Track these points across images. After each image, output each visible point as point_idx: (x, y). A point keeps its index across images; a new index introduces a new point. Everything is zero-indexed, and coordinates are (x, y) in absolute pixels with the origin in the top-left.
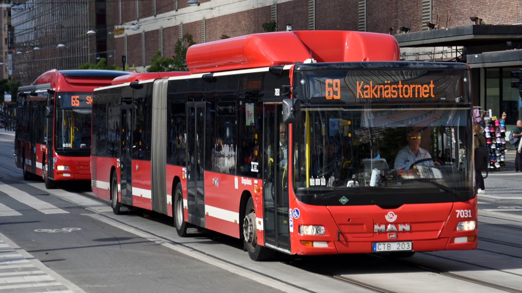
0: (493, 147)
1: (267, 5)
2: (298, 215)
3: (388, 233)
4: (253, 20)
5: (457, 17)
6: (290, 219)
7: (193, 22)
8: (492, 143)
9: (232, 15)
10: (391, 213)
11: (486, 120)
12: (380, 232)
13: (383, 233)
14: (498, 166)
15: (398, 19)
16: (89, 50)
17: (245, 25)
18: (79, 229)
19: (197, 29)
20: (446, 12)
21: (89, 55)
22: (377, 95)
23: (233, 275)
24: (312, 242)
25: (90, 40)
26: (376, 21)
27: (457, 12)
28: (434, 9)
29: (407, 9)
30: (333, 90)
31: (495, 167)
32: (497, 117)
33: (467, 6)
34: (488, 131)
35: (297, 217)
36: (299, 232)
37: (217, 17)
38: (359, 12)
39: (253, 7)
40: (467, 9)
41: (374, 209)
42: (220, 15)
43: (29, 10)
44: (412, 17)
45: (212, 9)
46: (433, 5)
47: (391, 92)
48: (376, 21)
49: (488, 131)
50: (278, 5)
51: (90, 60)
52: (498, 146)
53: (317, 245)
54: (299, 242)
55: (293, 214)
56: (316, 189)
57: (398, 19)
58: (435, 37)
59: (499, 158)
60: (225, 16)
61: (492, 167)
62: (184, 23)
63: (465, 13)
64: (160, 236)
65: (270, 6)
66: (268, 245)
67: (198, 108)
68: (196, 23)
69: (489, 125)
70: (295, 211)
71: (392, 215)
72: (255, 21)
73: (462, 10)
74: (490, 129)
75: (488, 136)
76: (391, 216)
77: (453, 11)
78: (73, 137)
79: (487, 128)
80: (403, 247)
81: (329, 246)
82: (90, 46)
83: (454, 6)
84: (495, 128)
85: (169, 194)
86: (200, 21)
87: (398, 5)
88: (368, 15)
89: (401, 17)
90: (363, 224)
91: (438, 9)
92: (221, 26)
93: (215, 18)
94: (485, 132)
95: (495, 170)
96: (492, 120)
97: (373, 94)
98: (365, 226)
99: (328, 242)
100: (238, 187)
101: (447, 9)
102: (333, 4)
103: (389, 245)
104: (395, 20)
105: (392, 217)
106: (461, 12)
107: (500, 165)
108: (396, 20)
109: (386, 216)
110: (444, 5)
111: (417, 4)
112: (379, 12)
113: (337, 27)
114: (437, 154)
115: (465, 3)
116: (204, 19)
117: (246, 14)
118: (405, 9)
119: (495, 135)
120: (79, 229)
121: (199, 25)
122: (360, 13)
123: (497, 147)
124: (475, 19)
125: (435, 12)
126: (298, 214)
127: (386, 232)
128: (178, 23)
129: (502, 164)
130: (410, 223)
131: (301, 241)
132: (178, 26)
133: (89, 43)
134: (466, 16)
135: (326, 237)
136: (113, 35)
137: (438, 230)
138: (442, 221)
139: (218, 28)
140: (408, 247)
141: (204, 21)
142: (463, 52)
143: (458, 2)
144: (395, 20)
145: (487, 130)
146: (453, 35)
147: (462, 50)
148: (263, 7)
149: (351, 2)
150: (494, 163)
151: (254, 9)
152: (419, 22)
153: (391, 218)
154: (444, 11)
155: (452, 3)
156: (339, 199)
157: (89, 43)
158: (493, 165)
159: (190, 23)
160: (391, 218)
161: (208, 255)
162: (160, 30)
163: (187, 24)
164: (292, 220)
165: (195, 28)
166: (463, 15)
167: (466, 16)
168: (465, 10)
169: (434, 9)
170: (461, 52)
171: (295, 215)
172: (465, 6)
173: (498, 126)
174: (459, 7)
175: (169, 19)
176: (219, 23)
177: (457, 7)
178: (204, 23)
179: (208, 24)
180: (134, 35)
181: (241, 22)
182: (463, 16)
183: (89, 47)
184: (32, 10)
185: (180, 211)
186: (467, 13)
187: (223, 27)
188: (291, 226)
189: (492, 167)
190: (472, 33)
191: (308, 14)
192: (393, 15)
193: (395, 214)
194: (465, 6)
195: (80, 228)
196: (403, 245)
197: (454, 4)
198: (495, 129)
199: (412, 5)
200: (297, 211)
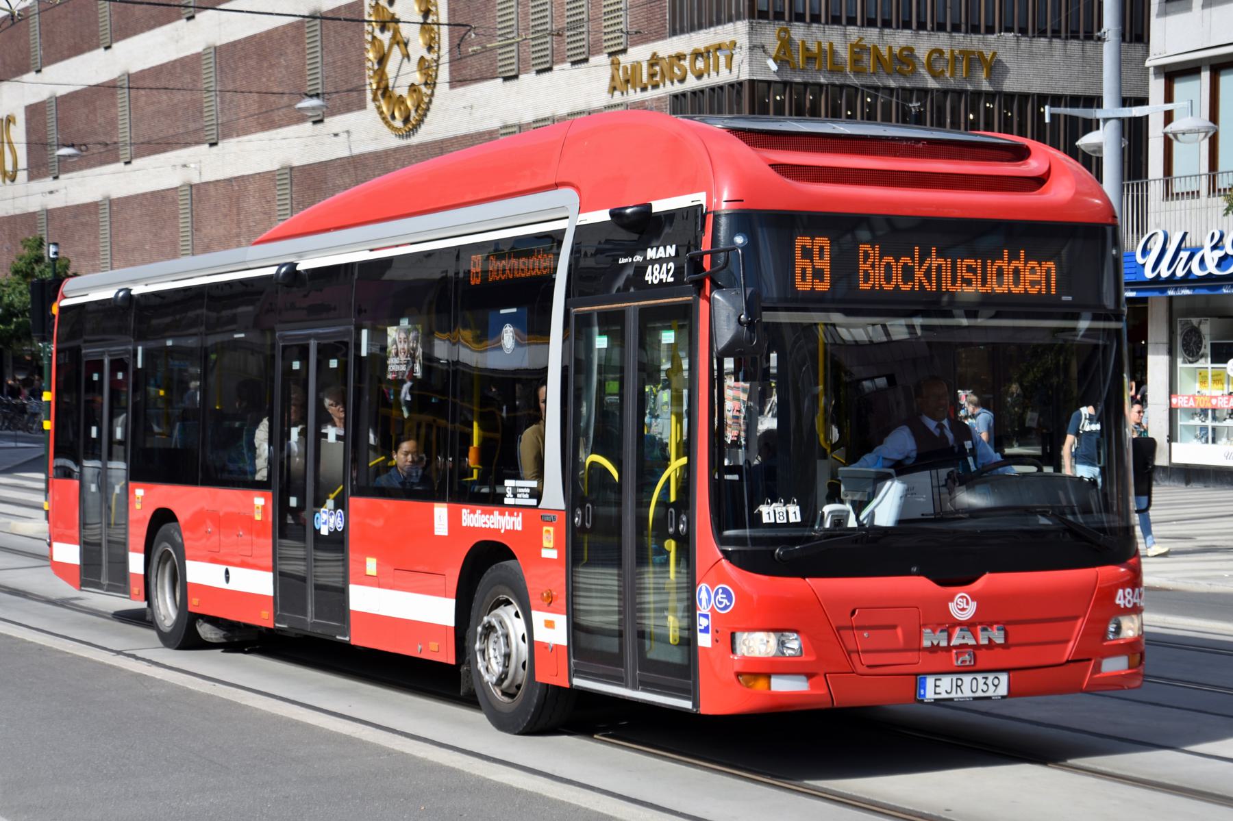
1: (31, 210)
2: (730, 601)
3: (954, 651)
6: (698, 612)
10: (962, 597)
12: (935, 649)
13: (943, 649)
22: (931, 285)
24: (768, 676)
30: (813, 266)
35: (726, 607)
36: (733, 650)
41: (917, 585)
47: (962, 276)
50: (48, 211)
53: (782, 685)
54: (733, 677)
55: (709, 599)
56: (783, 534)
66: (578, 682)
67: (112, 362)
70: (720, 591)
71: (965, 600)
72: (10, 235)
76: (962, 606)
80: (974, 689)
81: (811, 686)
85: (135, 550)
90: (894, 627)
97: (920, 280)
98: (899, 631)
99: (809, 676)
100: (447, 530)
102: (139, 212)
103: (959, 683)
105: (965, 607)
109: (950, 604)
114: (99, 487)
126: (729, 598)
127: (949, 649)
130: (1006, 626)
131: (738, 674)
135: (803, 663)
137: (1067, 641)
138: (1076, 618)
140: (985, 688)
153: (963, 609)
160: (963, 609)
164: (709, 614)
171: (721, 603)
185: (163, 588)
188: (706, 630)
191: (99, 226)
193: (973, 600)
196: (975, 681)
200: (725, 591)
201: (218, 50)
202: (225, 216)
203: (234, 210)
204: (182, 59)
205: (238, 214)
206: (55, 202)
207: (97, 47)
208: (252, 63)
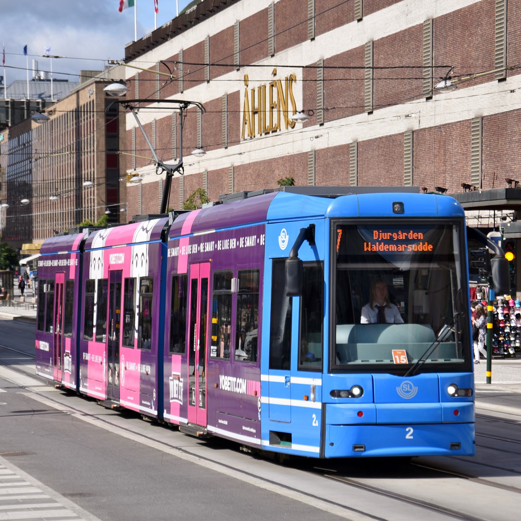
0: (507, 330)
1: (305, 151)
4: (288, 169)
5: (507, 175)
7: (220, 169)
8: (506, 326)
9: (264, 162)
11: (499, 300)
14: (511, 352)
15: (447, 175)
16: (96, 201)
17: (279, 175)
18: (5, 404)
19: (224, 178)
20: (497, 169)
21: (96, 207)
23: (107, 432)
25: (97, 189)
26: (423, 176)
27: (508, 169)
28: (484, 164)
29: (455, 163)
31: (509, 354)
32: (511, 296)
33: (518, 162)
34: (502, 312)
37: (248, 164)
38: (405, 164)
39: (288, 154)
40: (518, 166)
42: (251, 162)
43: (23, 146)
44: (461, 173)
45: (241, 154)
46: (483, 159)
48: (423, 176)
49: (502, 312)
51: (97, 214)
52: (513, 329)
57: (447, 175)
58: (468, 201)
59: (513, 342)
60: (256, 162)
61: (506, 353)
62: (209, 169)
63: (516, 170)
64: (77, 409)
65: (307, 153)
68: (222, 170)
69: (502, 305)
73: (513, 167)
74: (503, 310)
75: (501, 317)
77: (503, 168)
78: (117, 311)
79: (500, 308)
82: (98, 195)
83: (505, 161)
84: (509, 308)
86: (227, 169)
87: (447, 157)
88: (414, 168)
89: (449, 173)
91: (488, 164)
92: (252, 175)
93: (245, 164)
94: (497, 314)
95: (509, 356)
96: (506, 299)
101: (497, 165)
104: (444, 175)
106: (512, 169)
107: (515, 351)
108: (445, 175)
110: (494, 159)
111: (467, 158)
112: (426, 165)
113: (381, 181)
115: (515, 158)
116: (232, 165)
117: (281, 161)
118: (454, 163)
119: (509, 317)
120: (5, 404)
121: (226, 173)
122: (406, 165)
123: (511, 330)
124: (510, 181)
125: (485, 168)
128: (202, 170)
129: (516, 350)
132: (202, 173)
133: (96, 192)
134: (517, 174)
136: (124, 183)
139: (248, 177)
141: (232, 168)
142: (513, 216)
143: (508, 157)
144: (444, 175)
145: (500, 311)
146: (486, 199)
147: (512, 215)
148: (300, 154)
149: (396, 151)
150: (508, 348)
151: (289, 156)
152: (468, 180)
154: (494, 167)
155: (502, 158)
156: (47, 352)
157: (96, 192)
158: (507, 351)
159: (216, 170)
161: (108, 423)
162: (180, 178)
163: (213, 172)
165: (222, 177)
166: (514, 172)
167: (517, 174)
168: (515, 166)
169: (484, 164)
170: (511, 216)
172: (515, 162)
173: (513, 307)
174: (510, 163)
175: (190, 165)
176: (250, 171)
177: (507, 163)
178: (232, 171)
179: (236, 172)
180: (150, 183)
181: (274, 171)
182: (513, 174)
183: (96, 197)
184: (27, 147)
186: (518, 170)
187: (254, 177)
189: (506, 353)
190: (505, 198)
192: (441, 170)
194: (515, 162)
195: (5, 402)
197: (505, 159)
198: (509, 310)
199: (461, 158)
201: (434, 22)
202: (436, 156)
203: (442, 151)
204: (410, 29)
205: (445, 155)
206: (321, 144)
207: (353, 20)
208: (458, 32)
